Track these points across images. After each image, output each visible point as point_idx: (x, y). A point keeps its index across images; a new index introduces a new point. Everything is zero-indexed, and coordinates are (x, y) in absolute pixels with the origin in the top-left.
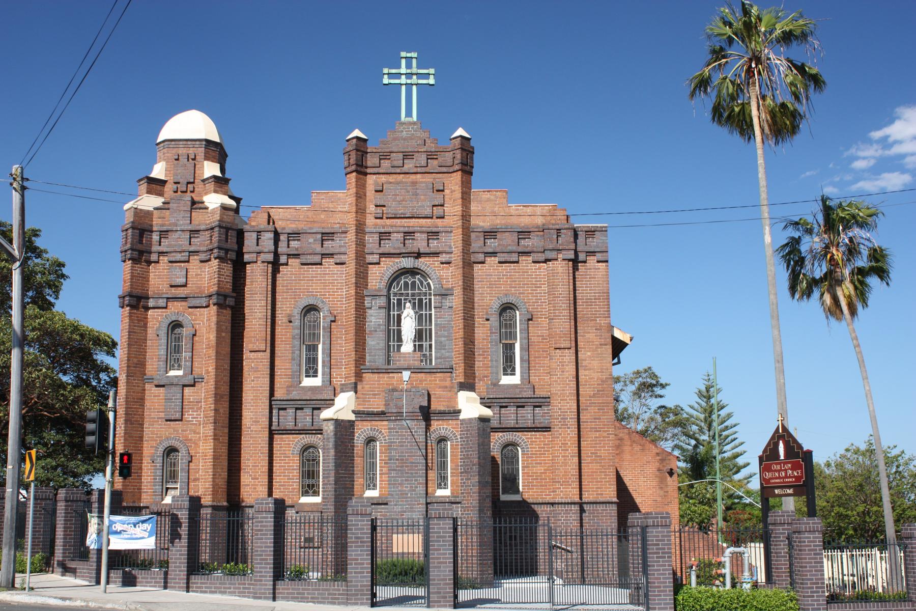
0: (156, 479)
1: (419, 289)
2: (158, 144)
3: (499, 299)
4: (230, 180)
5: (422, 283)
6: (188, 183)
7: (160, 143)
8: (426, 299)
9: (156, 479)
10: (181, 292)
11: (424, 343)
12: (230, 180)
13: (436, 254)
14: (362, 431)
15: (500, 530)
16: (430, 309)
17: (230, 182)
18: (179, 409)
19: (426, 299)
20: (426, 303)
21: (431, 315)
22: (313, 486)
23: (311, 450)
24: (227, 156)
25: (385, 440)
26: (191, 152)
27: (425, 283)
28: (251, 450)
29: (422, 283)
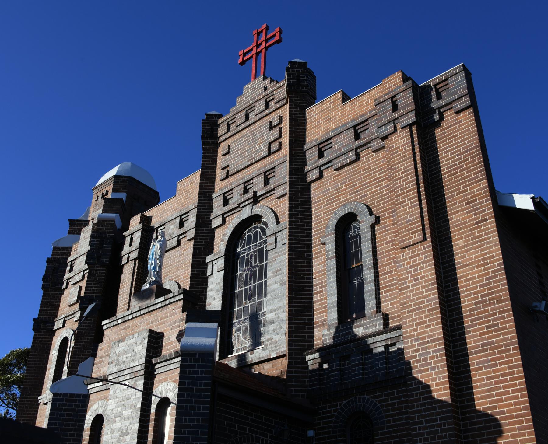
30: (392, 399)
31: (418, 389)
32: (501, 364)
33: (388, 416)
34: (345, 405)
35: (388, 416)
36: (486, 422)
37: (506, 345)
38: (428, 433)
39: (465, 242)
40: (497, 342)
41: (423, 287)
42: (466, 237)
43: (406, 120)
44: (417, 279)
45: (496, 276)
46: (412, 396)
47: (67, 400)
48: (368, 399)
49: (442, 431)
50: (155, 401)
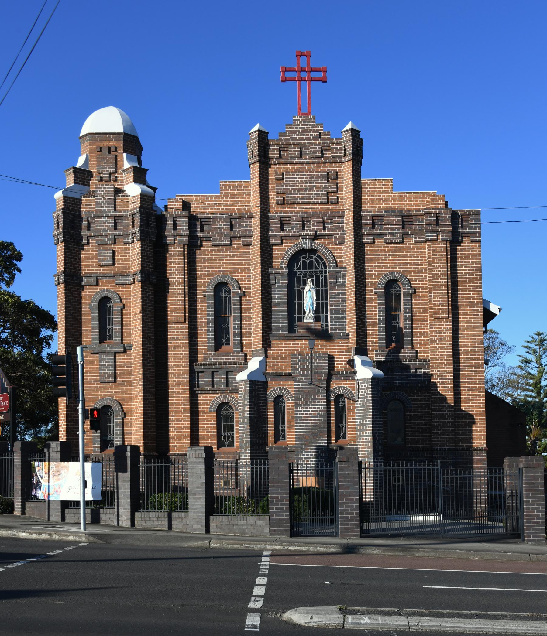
0: (209, 324)
1: (316, 268)
2: (81, 138)
3: (386, 276)
4: (147, 170)
5: (318, 262)
6: (110, 174)
7: (84, 136)
8: (322, 276)
9: (209, 324)
10: (110, 270)
11: (321, 315)
12: (147, 170)
13: (330, 236)
14: (273, 388)
15: (257, 471)
16: (326, 286)
17: (147, 172)
18: (111, 373)
19: (322, 276)
20: (322, 280)
21: (326, 290)
22: (228, 438)
23: (226, 407)
24: (142, 149)
25: (291, 398)
26: (112, 143)
27: (321, 262)
28: (175, 408)
29: (318, 262)
30: (417, 396)
31: (437, 395)
32: (475, 390)
33: (413, 404)
34: (388, 394)
35: (413, 404)
36: (465, 414)
37: (479, 382)
38: (440, 417)
39: (466, 323)
40: (475, 379)
41: (445, 344)
42: (466, 321)
43: (445, 236)
44: (441, 339)
45: (479, 347)
46: (434, 398)
47: (256, 385)
48: (403, 394)
49: (448, 416)
50: (333, 396)
